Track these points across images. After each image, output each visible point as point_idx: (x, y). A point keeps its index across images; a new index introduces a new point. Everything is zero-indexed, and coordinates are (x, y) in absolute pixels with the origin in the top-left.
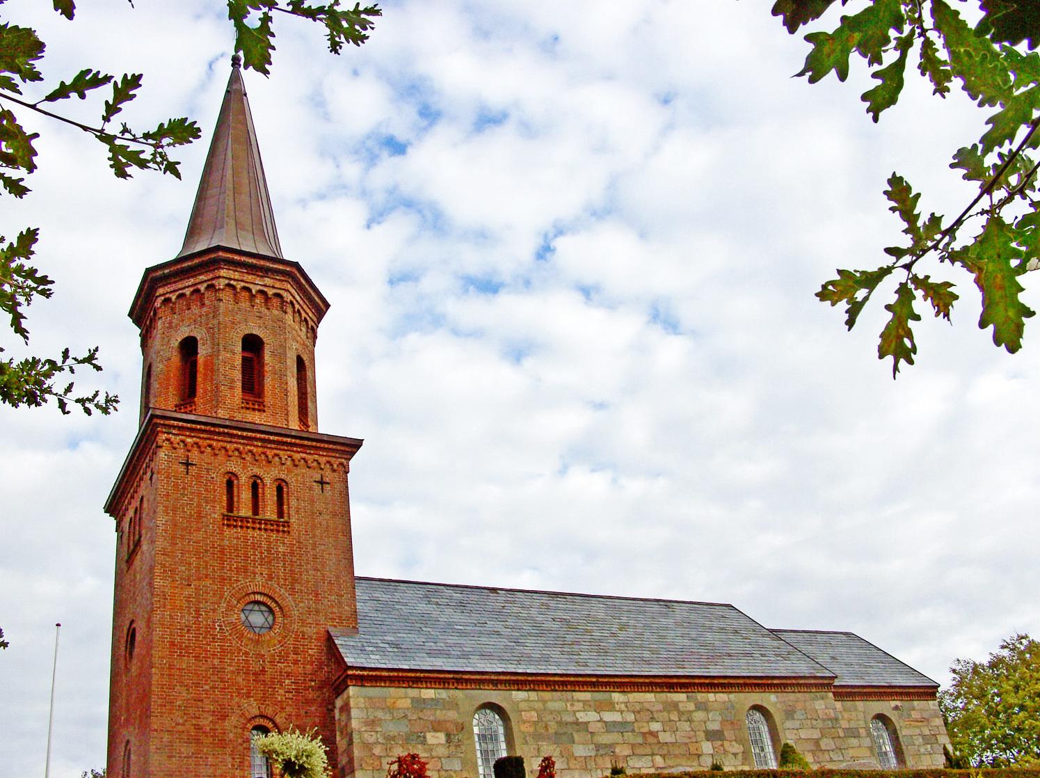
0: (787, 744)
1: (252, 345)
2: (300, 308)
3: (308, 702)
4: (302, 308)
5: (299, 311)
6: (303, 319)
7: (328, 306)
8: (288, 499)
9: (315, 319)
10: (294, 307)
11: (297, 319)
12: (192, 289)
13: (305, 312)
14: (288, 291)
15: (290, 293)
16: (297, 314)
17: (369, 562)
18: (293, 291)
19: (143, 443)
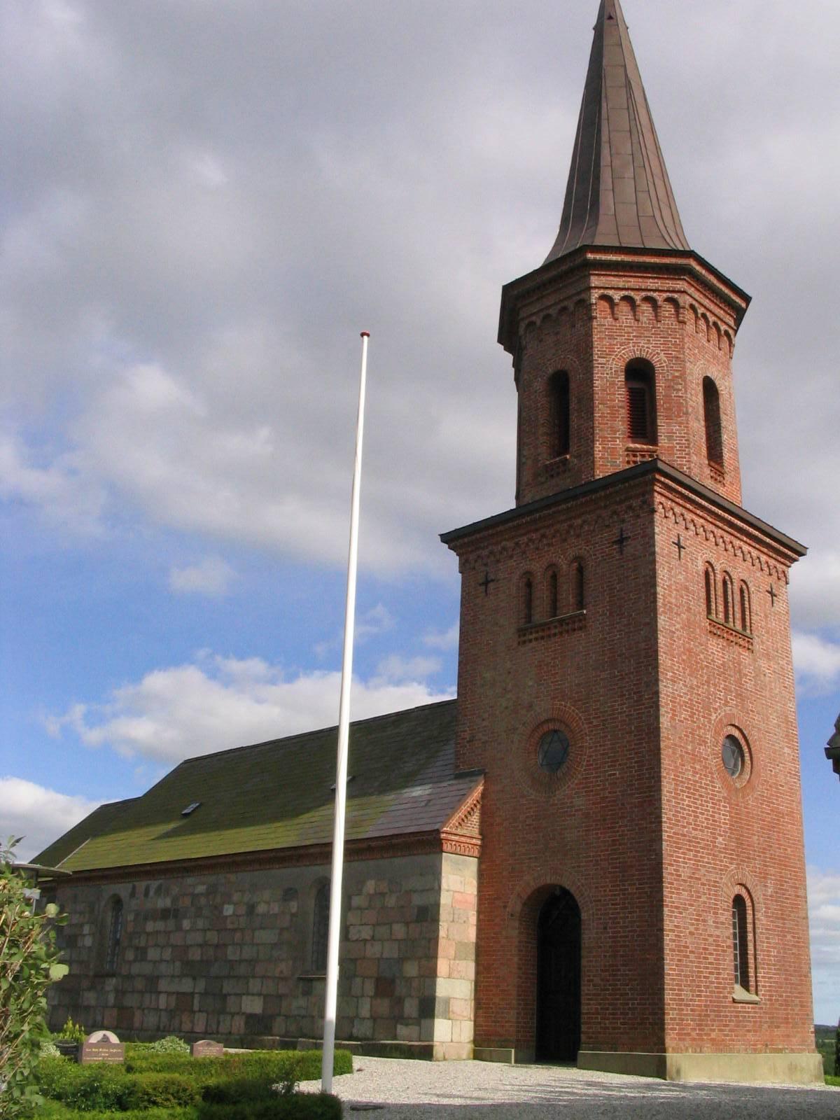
0: (207, 1088)
1: (640, 374)
2: (727, 328)
3: (522, 951)
4: (708, 310)
5: (715, 324)
6: (723, 332)
7: (747, 299)
8: (750, 615)
9: (732, 323)
10: (718, 329)
11: (714, 335)
12: (542, 315)
13: (702, 305)
14: (684, 292)
15: (690, 294)
16: (725, 338)
17: (513, 506)
18: (691, 291)
19: (478, 536)
